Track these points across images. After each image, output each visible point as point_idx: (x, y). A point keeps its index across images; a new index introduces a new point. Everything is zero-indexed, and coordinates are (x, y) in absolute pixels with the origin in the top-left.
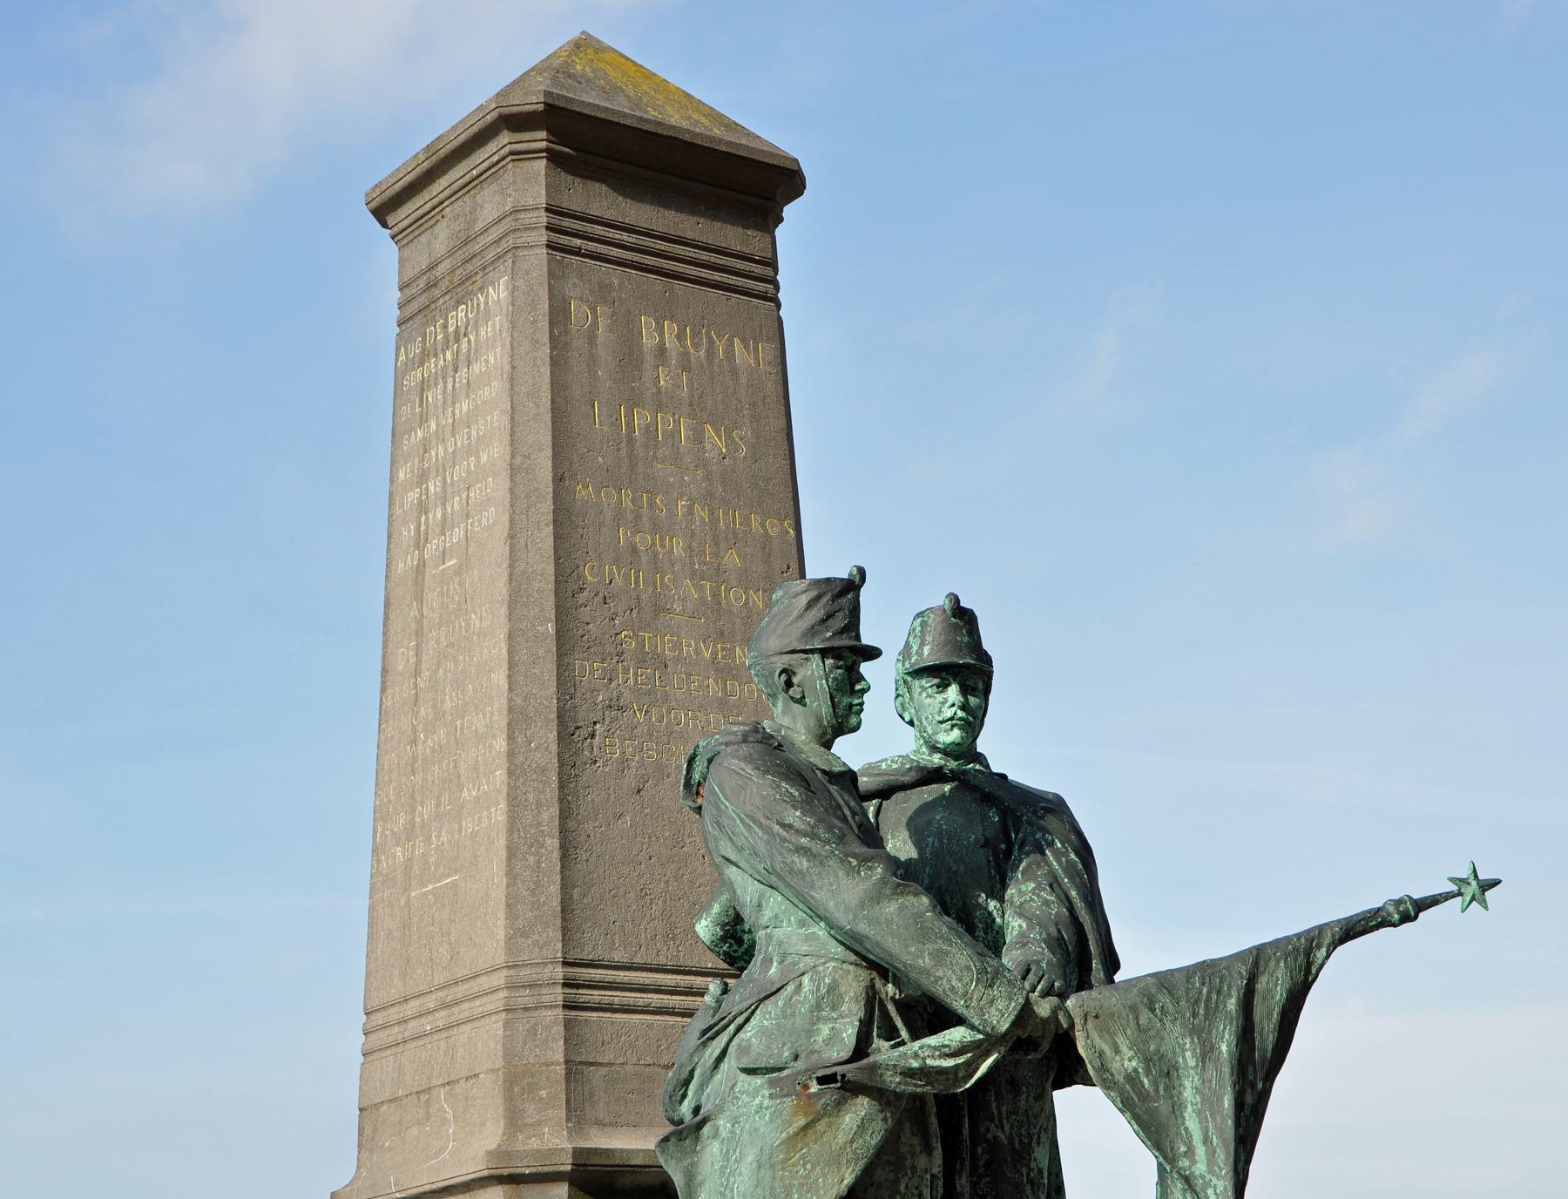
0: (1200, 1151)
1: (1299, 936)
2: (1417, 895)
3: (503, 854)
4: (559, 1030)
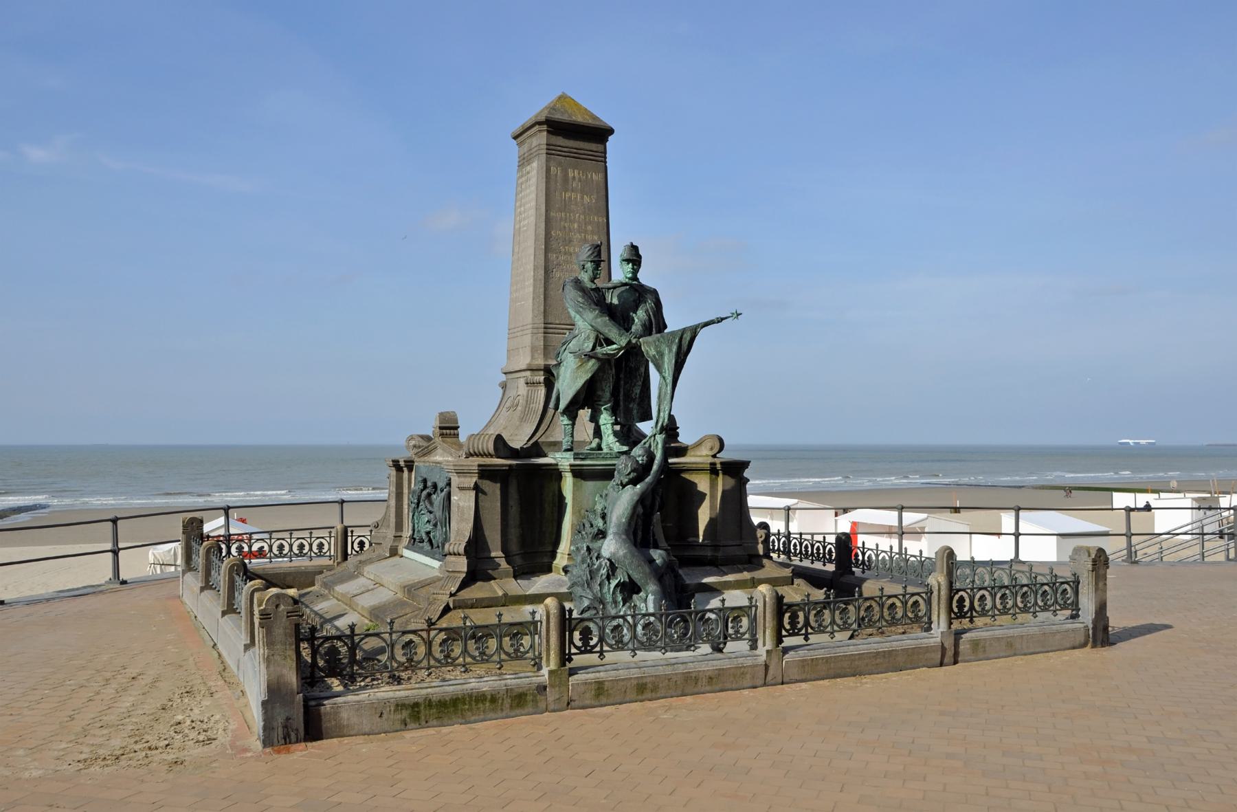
0: (667, 372)
2: (722, 317)
3: (532, 298)
4: (542, 338)
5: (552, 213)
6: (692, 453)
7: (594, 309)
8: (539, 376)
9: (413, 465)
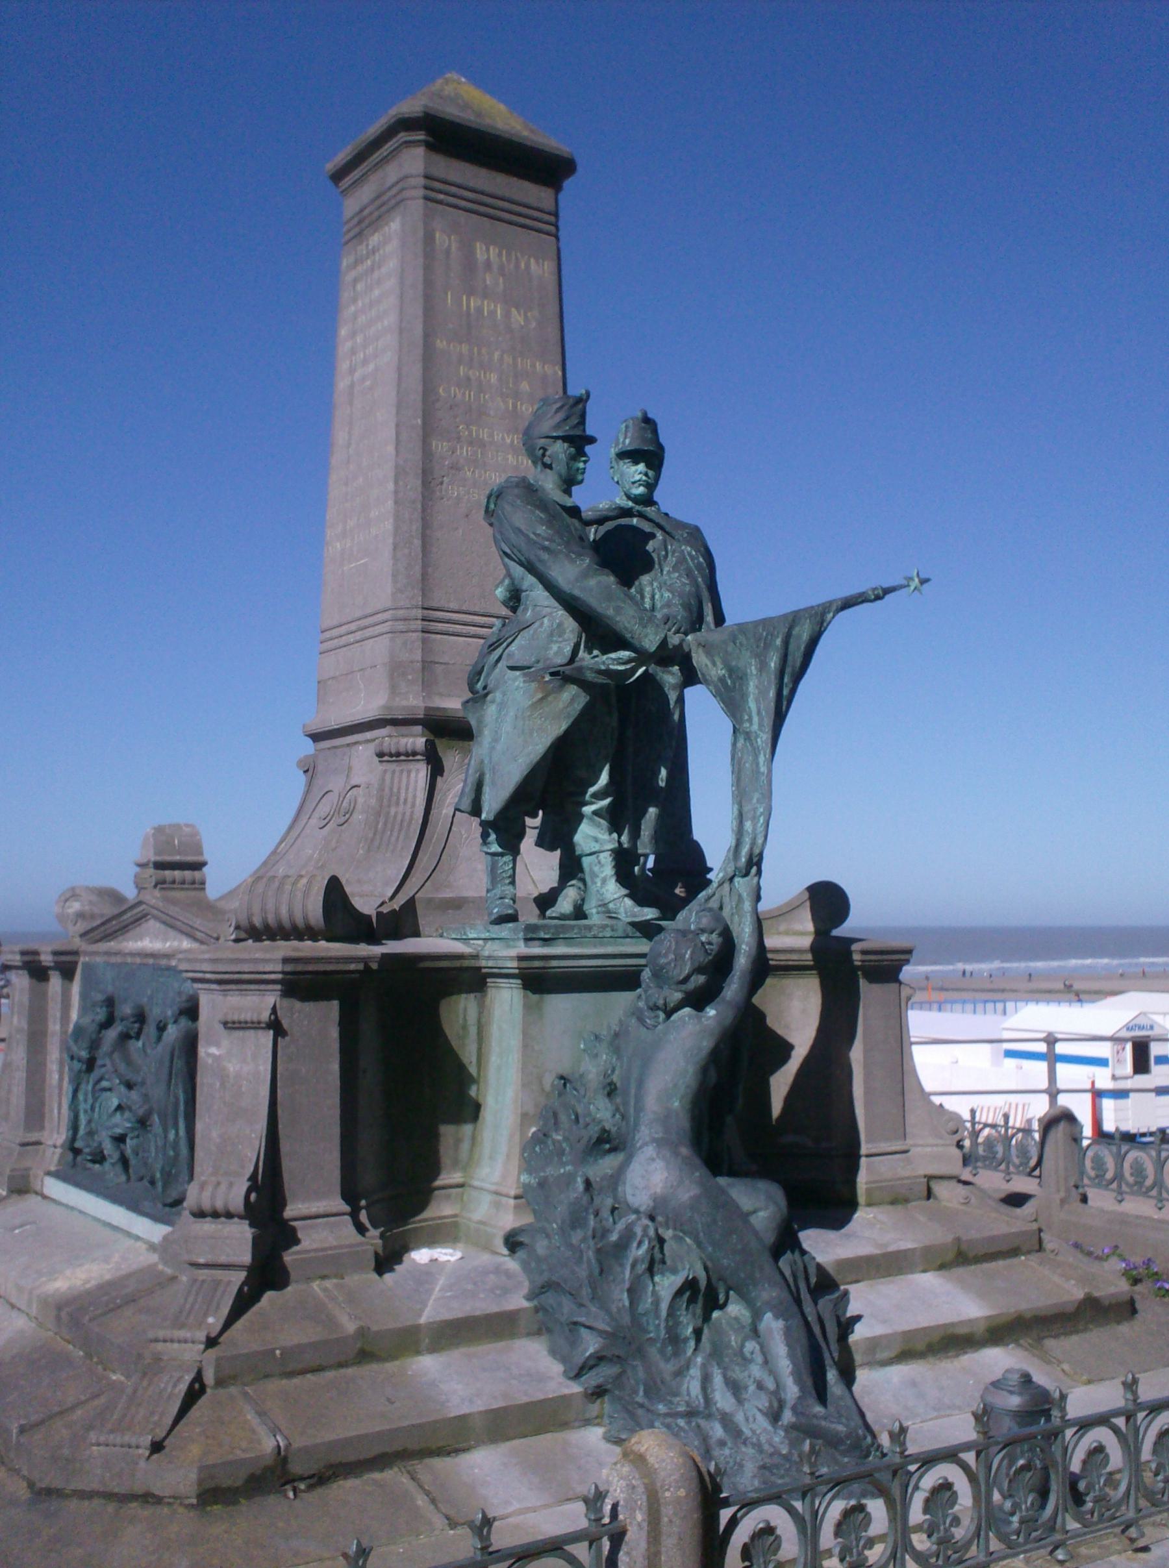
0: (756, 719)
1: (818, 606)
2: (885, 585)
3: (391, 547)
7: (579, 555)
9: (76, 963)
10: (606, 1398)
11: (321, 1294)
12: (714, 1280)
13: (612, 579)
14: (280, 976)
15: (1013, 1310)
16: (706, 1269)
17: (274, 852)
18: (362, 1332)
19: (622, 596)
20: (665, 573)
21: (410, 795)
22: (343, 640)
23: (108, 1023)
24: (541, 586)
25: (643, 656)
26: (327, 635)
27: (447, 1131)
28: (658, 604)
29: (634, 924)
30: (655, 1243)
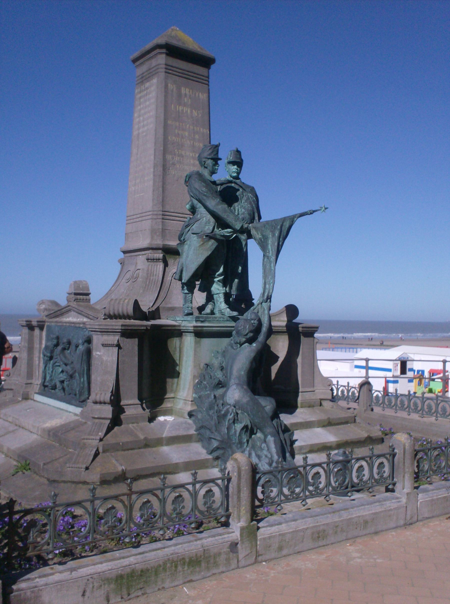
0: (271, 252)
1: (292, 216)
2: (314, 209)
5: (169, 121)
6: (277, 319)
8: (158, 253)
10: (219, 460)
11: (132, 428)
12: (253, 426)
13: (226, 206)
14: (120, 330)
15: (345, 439)
16: (251, 422)
17: (110, 290)
18: (146, 439)
19: (229, 211)
20: (242, 202)
21: (157, 273)
22: (135, 220)
23: (57, 345)
24: (203, 207)
25: (235, 231)
26: (129, 218)
27: (169, 380)
28: (240, 213)
29: (229, 317)
30: (235, 414)
